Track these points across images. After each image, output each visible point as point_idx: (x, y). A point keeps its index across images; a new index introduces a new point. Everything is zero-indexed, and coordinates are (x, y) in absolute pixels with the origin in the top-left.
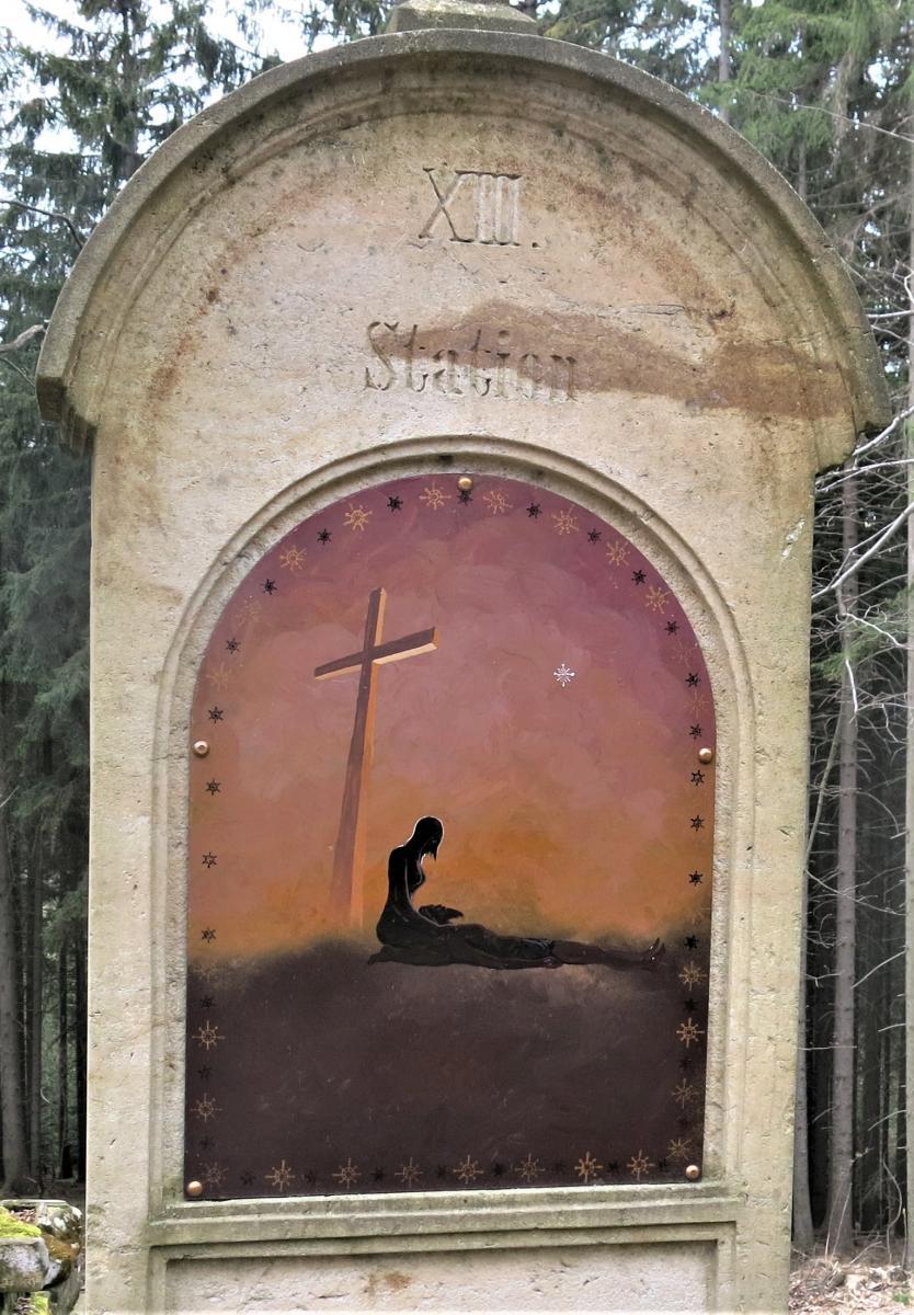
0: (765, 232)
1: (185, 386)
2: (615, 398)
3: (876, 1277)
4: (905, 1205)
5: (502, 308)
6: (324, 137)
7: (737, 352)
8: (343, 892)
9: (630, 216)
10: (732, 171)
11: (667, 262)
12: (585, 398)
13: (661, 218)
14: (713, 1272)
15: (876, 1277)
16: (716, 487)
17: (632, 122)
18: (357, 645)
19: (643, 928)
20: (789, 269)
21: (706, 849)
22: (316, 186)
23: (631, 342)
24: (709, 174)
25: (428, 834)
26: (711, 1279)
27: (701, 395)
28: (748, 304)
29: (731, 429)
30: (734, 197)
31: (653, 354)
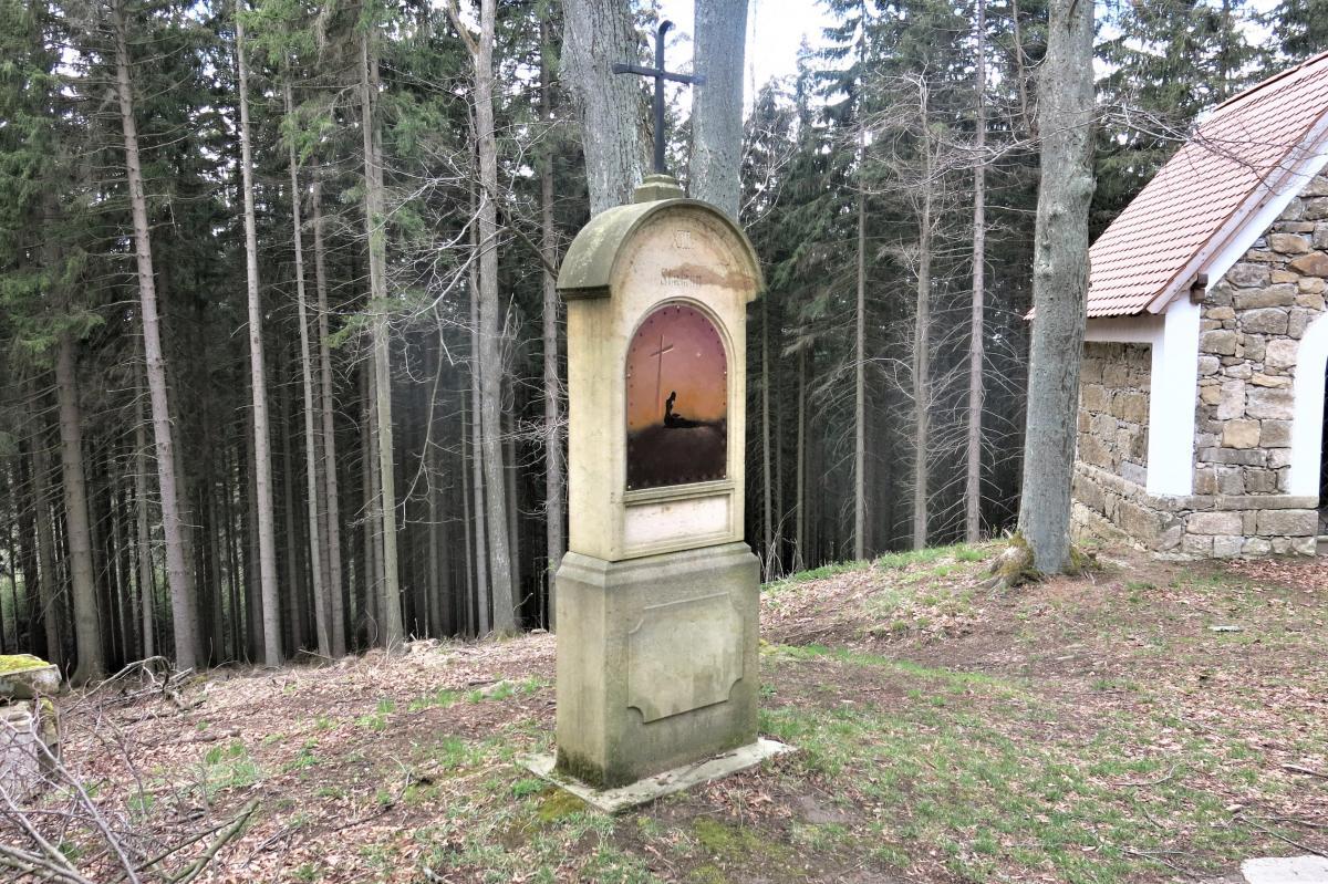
0: (739, 246)
1: (627, 286)
2: (709, 286)
3: (426, 645)
4: (401, 597)
5: (688, 264)
6: (653, 223)
7: (731, 274)
8: (657, 410)
9: (710, 241)
10: (734, 230)
11: (718, 252)
12: (703, 286)
13: (716, 241)
14: (728, 503)
15: (426, 645)
16: (728, 307)
17: (713, 219)
18: (658, 349)
19: (714, 417)
20: (744, 255)
21: (725, 397)
22: (651, 235)
23: (711, 272)
24: (728, 232)
25: (674, 395)
26: (728, 503)
27: (725, 286)
28: (733, 262)
29: (730, 293)
30: (733, 237)
31: (715, 275)
